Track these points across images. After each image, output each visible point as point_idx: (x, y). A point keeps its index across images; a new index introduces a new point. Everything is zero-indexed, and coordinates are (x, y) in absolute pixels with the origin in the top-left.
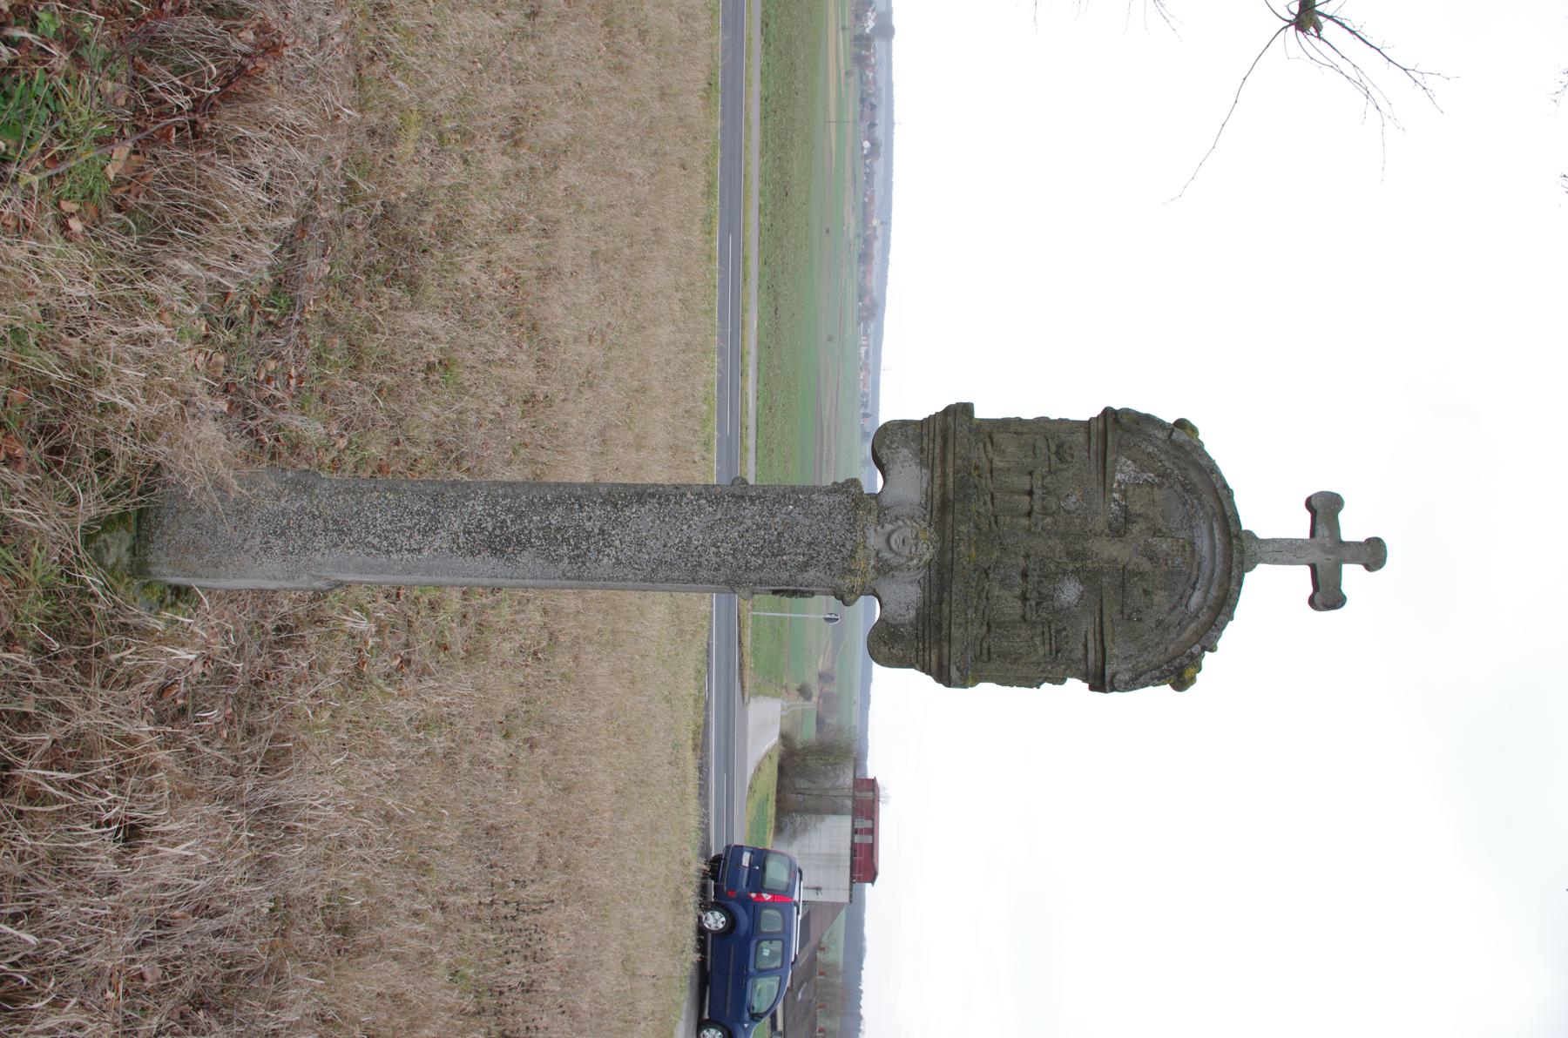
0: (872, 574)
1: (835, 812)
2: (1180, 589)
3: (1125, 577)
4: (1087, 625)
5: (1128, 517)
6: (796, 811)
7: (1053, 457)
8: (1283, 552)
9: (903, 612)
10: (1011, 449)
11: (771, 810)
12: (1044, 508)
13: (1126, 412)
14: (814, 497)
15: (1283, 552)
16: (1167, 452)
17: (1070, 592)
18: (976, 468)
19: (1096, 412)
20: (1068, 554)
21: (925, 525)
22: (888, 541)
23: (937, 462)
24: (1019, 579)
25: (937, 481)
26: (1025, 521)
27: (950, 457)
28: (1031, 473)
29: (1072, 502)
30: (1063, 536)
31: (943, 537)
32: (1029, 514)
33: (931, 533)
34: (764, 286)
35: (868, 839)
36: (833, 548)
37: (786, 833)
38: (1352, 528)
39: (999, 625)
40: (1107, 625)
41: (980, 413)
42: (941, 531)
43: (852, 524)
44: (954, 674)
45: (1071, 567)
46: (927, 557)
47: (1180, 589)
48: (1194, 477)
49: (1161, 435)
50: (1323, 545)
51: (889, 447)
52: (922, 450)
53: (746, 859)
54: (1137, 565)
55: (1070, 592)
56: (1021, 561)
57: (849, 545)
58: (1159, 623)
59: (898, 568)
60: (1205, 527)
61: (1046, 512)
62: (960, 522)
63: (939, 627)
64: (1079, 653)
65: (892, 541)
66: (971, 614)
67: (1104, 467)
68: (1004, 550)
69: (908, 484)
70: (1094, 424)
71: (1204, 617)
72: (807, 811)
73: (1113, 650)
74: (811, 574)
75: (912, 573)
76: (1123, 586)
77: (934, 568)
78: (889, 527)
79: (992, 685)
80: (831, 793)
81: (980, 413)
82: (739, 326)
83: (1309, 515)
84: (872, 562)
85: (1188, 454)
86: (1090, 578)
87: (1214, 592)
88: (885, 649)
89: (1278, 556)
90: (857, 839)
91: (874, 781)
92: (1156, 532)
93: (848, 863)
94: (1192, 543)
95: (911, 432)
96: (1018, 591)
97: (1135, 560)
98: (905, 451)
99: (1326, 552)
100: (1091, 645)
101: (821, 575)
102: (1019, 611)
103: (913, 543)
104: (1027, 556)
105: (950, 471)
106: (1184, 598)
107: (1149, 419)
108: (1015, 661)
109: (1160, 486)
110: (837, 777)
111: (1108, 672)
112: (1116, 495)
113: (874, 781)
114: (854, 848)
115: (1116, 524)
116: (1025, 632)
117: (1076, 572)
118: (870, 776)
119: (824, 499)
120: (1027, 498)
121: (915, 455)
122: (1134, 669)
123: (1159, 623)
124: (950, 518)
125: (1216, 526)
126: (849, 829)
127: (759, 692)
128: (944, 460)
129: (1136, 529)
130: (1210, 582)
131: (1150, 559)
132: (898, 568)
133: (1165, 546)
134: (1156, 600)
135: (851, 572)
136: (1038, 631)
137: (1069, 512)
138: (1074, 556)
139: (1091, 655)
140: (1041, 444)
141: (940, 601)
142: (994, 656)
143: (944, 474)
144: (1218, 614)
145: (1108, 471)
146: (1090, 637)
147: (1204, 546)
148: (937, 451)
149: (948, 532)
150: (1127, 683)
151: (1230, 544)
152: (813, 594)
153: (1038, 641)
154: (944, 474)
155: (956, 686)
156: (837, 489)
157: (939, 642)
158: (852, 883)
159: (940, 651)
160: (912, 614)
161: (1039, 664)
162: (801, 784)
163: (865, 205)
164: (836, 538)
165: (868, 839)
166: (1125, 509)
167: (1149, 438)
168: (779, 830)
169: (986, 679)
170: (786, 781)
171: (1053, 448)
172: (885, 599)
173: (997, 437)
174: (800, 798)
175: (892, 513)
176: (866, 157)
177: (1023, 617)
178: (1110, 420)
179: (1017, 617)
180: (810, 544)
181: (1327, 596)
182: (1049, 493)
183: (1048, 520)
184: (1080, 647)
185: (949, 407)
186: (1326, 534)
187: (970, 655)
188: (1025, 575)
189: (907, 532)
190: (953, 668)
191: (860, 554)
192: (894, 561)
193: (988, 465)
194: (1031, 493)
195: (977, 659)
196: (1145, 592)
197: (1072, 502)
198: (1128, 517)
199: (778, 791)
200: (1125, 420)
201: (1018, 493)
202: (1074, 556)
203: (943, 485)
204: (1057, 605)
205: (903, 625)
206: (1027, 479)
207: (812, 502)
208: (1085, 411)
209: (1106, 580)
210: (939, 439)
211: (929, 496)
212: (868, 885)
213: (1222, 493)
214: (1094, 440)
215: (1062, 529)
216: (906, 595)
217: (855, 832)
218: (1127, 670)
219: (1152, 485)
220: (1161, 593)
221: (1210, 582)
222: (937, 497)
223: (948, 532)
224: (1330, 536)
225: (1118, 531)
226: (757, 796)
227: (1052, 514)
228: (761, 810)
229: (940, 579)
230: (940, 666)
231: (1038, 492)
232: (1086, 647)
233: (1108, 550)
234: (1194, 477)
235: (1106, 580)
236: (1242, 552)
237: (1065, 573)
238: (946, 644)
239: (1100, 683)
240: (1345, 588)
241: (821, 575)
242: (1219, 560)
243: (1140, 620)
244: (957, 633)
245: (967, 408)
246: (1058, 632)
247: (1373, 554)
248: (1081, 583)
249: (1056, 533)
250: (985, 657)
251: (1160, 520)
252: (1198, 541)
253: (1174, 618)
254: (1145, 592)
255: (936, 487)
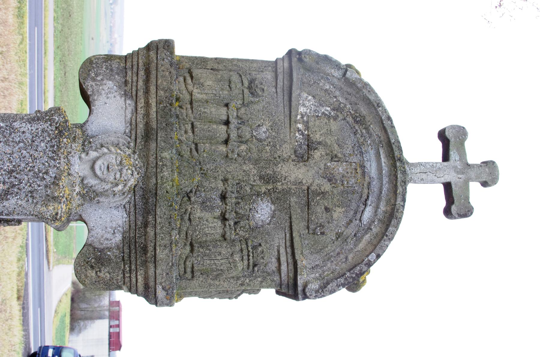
0: (77, 200)
1: (101, 318)
2: (354, 206)
3: (309, 196)
4: (279, 240)
5: (310, 145)
6: (80, 319)
7: (246, 91)
8: (427, 172)
9: (109, 236)
10: (210, 83)
11: (68, 320)
12: (239, 136)
13: (308, 52)
14: (16, 125)
15: (427, 172)
16: (341, 89)
17: (263, 211)
18: (178, 99)
19: (281, 53)
20: (261, 178)
21: (129, 152)
22: (93, 168)
23: (141, 93)
24: (219, 202)
25: (141, 111)
26: (223, 148)
27: (153, 89)
28: (227, 105)
29: (263, 132)
30: (256, 162)
31: (147, 164)
32: (226, 142)
33: (135, 160)
34: (58, 59)
35: (117, 330)
36: (36, 175)
37: (76, 331)
38: (475, 153)
39: (202, 245)
40: (296, 239)
41: (180, 51)
42: (145, 157)
43: (55, 151)
44: (161, 294)
45: (263, 189)
46: (132, 182)
47: (354, 206)
48: (364, 110)
49: (337, 74)
50: (455, 167)
51: (94, 80)
52: (126, 83)
53: (50, 352)
54: (319, 186)
55: (263, 211)
56: (220, 185)
57: (52, 172)
58: (339, 236)
59: (102, 194)
60: (372, 153)
61: (241, 140)
62: (163, 149)
63: (145, 250)
64: (273, 266)
65: (97, 167)
66: (175, 235)
67: (290, 101)
68: (204, 175)
69: (113, 113)
70: (280, 64)
71: (376, 229)
72: (86, 319)
73: (302, 262)
74: (11, 203)
75: (117, 198)
76: (308, 205)
77: (139, 193)
78: (93, 154)
79: (196, 299)
80: (98, 309)
81: (180, 51)
82: (41, 77)
83: (440, 144)
84: (77, 189)
85: (359, 90)
86: (279, 198)
87: (383, 207)
88: (92, 273)
89: (424, 176)
90: (112, 330)
91: (119, 302)
92: (334, 158)
93: (107, 342)
94: (363, 167)
95: (115, 65)
96: (218, 213)
97: (317, 181)
98: (110, 84)
99: (458, 173)
100: (283, 259)
101: (23, 203)
102: (220, 231)
103: (115, 168)
104: (225, 180)
105: (153, 102)
106: (358, 213)
107: (326, 59)
108: (217, 277)
109: (335, 118)
110: (101, 301)
111: (300, 282)
112: (300, 126)
113: (119, 302)
114: (110, 335)
115: (300, 151)
116: (225, 250)
117: (268, 193)
118: (117, 300)
119: (26, 127)
120: (224, 128)
121: (120, 87)
122: (321, 277)
123: (339, 236)
124: (153, 145)
125: (381, 151)
126: (107, 326)
127: (58, 262)
128: (147, 92)
129: (317, 154)
130: (379, 198)
131: (330, 180)
132: (102, 194)
133: (340, 169)
134: (335, 215)
135: (55, 199)
136: (238, 248)
137: (260, 140)
138: (266, 179)
139: (284, 267)
140: (235, 78)
141: (146, 225)
142: (197, 274)
143: (147, 104)
144: (388, 226)
145: (293, 104)
146: (282, 251)
147: (372, 169)
148: (141, 83)
149: (152, 159)
150: (317, 291)
151: (395, 167)
152: (19, 222)
153: (237, 257)
154: (147, 104)
155: (162, 304)
156: (39, 117)
157: (145, 263)
158: (109, 351)
159: (146, 273)
160: (119, 237)
161: (238, 278)
162: (83, 306)
163: (111, 27)
164: (38, 165)
165: (117, 330)
166: (308, 138)
167: (327, 77)
168: (72, 329)
169: (190, 294)
170: (75, 305)
171: (246, 84)
172: (91, 225)
173: (196, 72)
174: (83, 313)
175: (97, 142)
176: (111, 4)
177: (224, 236)
178: (295, 60)
179: (218, 237)
180: (11, 172)
181: (455, 205)
182: (243, 123)
183: (243, 147)
184: (274, 260)
185: (152, 42)
186: (457, 158)
187: (175, 274)
188: (223, 197)
189: (112, 159)
190: (159, 289)
191: (64, 181)
192: (100, 187)
193: (188, 97)
194: (227, 123)
195: (181, 277)
196: (327, 209)
197: (263, 132)
198: (310, 145)
199: (71, 310)
200: (307, 60)
201: (215, 122)
202: (266, 179)
203: (147, 115)
204: (252, 223)
205: (110, 249)
206: (224, 110)
207: (13, 130)
208: (273, 52)
209: (293, 199)
210: (142, 73)
211: (133, 125)
212: (118, 352)
213: (386, 123)
214: (280, 77)
215: (255, 155)
216: (109, 221)
217: (111, 327)
218: (316, 279)
219: (329, 117)
220: (339, 210)
221: (379, 198)
222: (141, 126)
223: (152, 159)
224: (460, 160)
225: (303, 156)
226: (60, 315)
227: (246, 142)
228: (62, 321)
229: (145, 202)
230: (147, 286)
231: (234, 122)
232: (279, 260)
233: (295, 173)
234: (364, 110)
235: (293, 199)
236: (404, 172)
237: (258, 194)
238: (151, 266)
239: (292, 290)
240: (473, 201)
241: (23, 203)
242: (385, 180)
243: (323, 233)
244: (161, 254)
245: (168, 45)
246: (255, 248)
247: (488, 173)
248: (273, 203)
249: (250, 159)
250: (189, 275)
251: (336, 146)
252: (367, 164)
253: (351, 231)
254: (327, 209)
255: (140, 117)
